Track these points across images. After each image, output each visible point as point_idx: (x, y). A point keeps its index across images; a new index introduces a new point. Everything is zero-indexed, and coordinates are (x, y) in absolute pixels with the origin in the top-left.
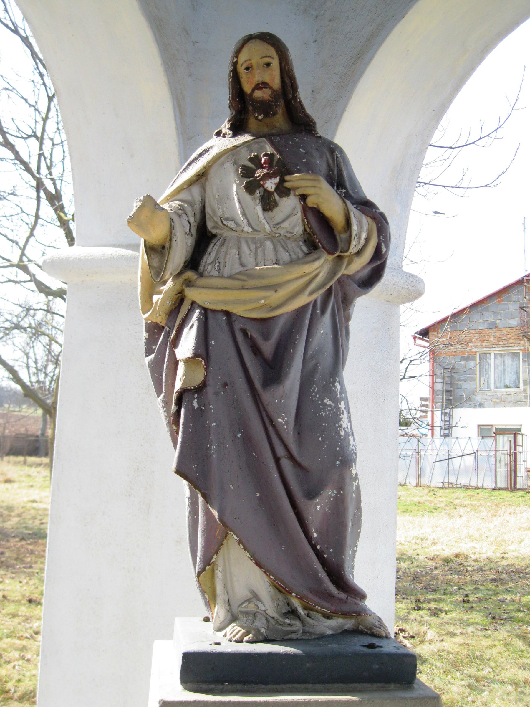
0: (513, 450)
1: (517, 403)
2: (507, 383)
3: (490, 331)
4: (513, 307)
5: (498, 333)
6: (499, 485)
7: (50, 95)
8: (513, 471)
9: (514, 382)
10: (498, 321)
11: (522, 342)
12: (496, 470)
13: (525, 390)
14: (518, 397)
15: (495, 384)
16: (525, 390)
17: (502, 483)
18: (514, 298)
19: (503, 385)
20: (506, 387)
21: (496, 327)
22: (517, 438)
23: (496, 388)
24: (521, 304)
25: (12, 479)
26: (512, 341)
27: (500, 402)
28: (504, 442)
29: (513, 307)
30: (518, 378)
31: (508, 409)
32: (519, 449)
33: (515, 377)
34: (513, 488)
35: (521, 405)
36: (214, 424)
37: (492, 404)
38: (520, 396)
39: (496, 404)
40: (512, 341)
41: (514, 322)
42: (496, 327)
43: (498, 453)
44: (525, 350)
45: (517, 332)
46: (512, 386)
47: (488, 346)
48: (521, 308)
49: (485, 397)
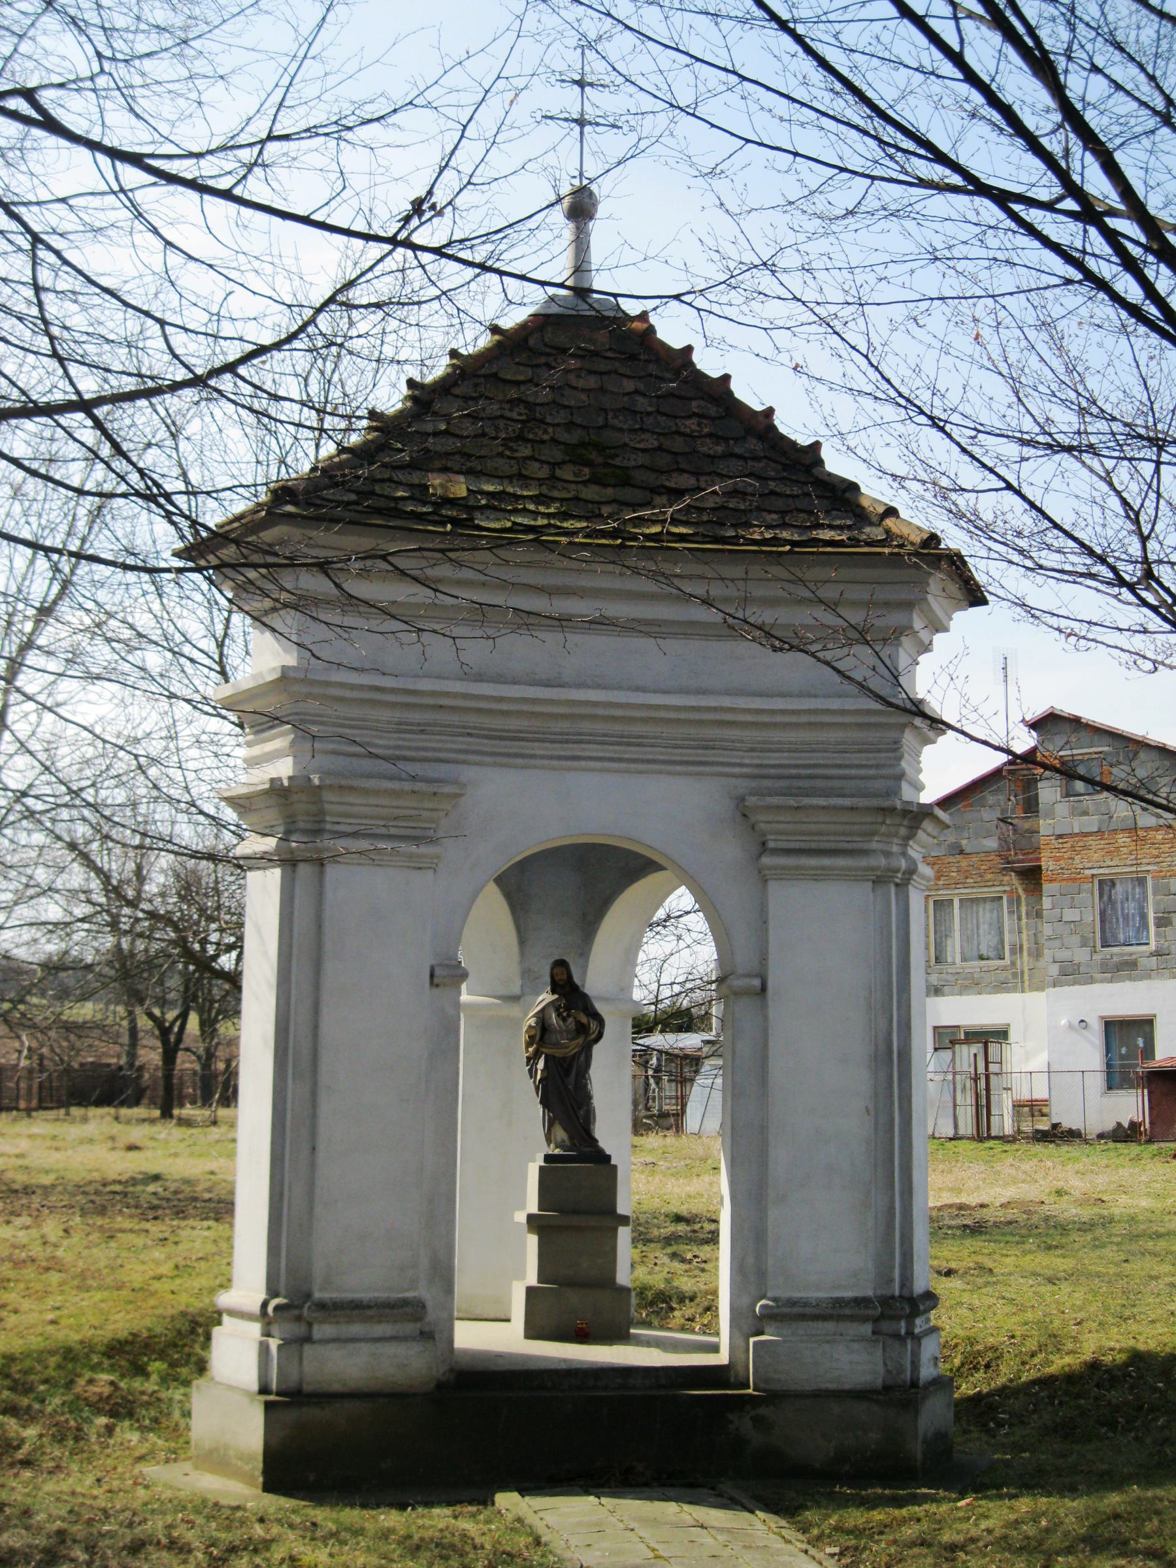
0: (981, 1069)
1: (1001, 987)
2: (984, 952)
3: (951, 859)
4: (990, 815)
5: (964, 864)
6: (962, 1132)
7: (174, 497)
8: (983, 1107)
9: (996, 949)
10: (964, 842)
11: (1006, 878)
12: (955, 1106)
13: (1013, 963)
14: (1003, 976)
15: (962, 953)
16: (1013, 963)
17: (967, 1126)
18: (991, 799)
19: (975, 954)
20: (981, 958)
21: (961, 852)
22: (990, 1050)
23: (964, 959)
24: (1003, 811)
25: (139, 1144)
26: (989, 876)
27: (972, 985)
28: (967, 1054)
29: (990, 815)
30: (1002, 942)
31: (985, 997)
32: (993, 1068)
33: (996, 940)
34: (982, 1134)
35: (1008, 990)
36: (312, 1479)
37: (956, 988)
38: (1005, 974)
39: (963, 990)
40: (989, 876)
41: (992, 844)
42: (961, 852)
43: (958, 1077)
44: (1011, 891)
45: (998, 860)
46: (991, 955)
47: (946, 886)
48: (1002, 820)
49: (944, 976)
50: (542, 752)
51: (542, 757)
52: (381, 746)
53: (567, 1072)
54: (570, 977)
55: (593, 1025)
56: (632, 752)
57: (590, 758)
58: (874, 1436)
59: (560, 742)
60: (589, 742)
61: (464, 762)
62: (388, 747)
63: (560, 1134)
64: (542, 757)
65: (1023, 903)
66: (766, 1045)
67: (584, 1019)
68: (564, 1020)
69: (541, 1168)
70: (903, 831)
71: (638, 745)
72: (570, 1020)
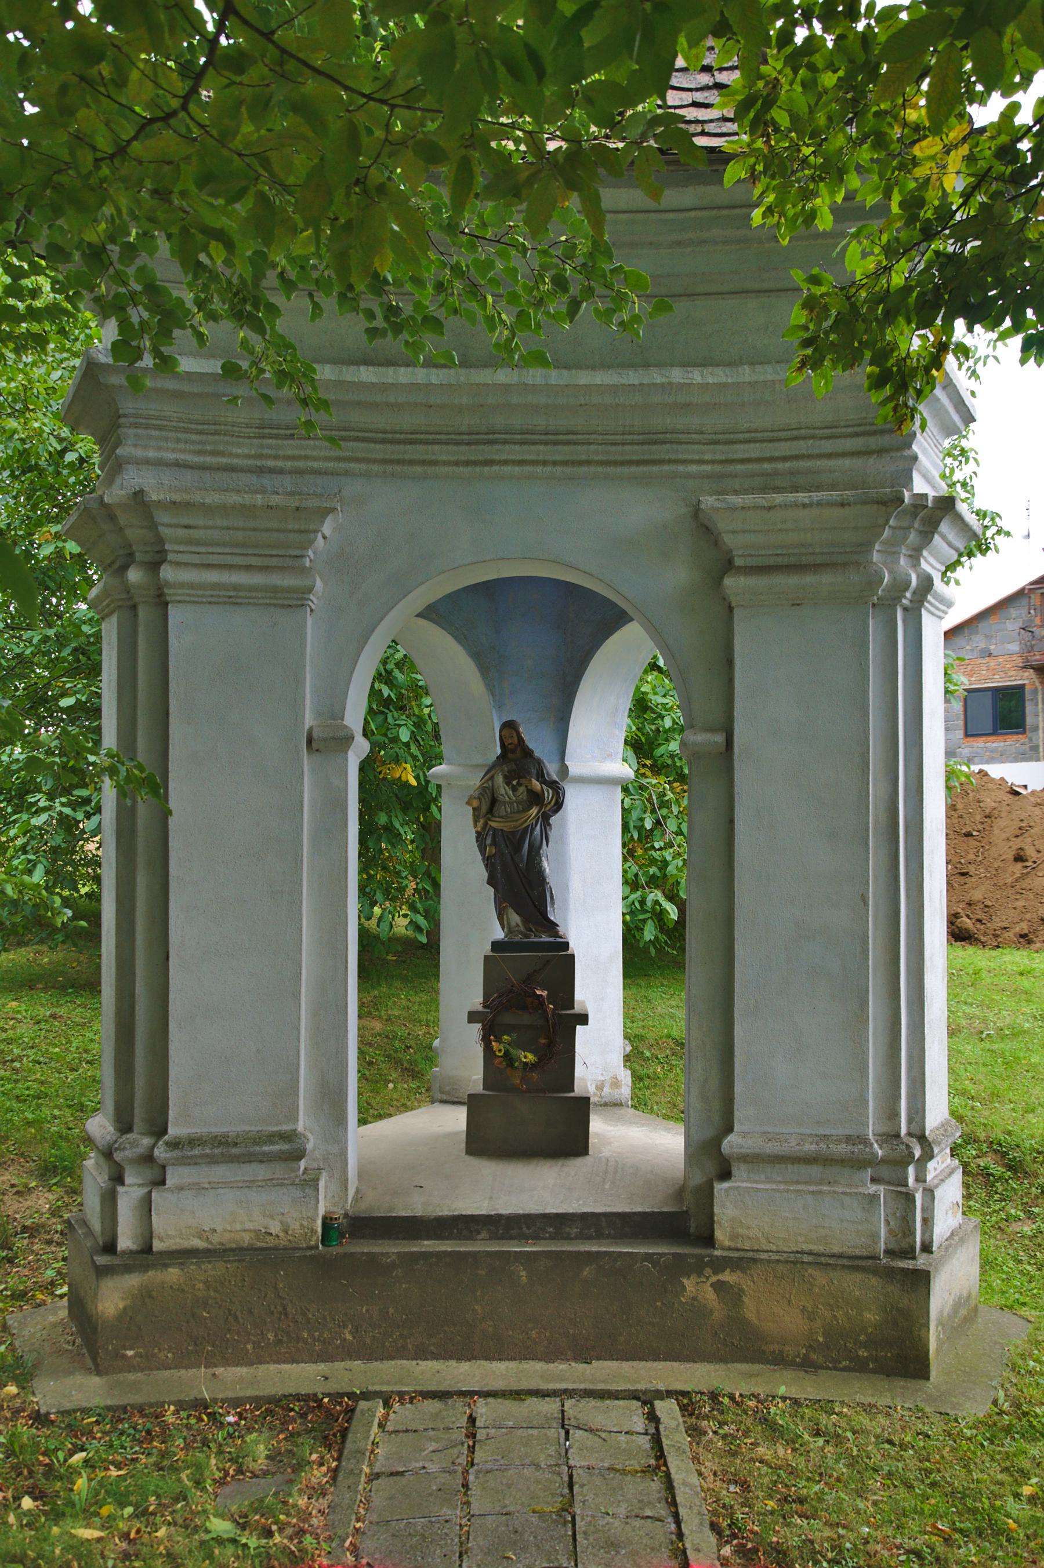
3: (980, 661)
10: (992, 647)
11: (1026, 674)
21: (990, 655)
26: (1013, 673)
40: (1013, 673)
41: (1015, 647)
42: (990, 655)
50: (444, 458)
51: (445, 463)
52: (238, 456)
53: (518, 848)
54: (521, 740)
55: (548, 794)
56: (563, 452)
57: (506, 462)
58: (871, 1316)
59: (469, 444)
60: (505, 442)
61: (347, 473)
62: (247, 456)
63: (515, 918)
64: (445, 463)
65: (740, 1184)
66: (732, 821)
67: (536, 785)
68: (514, 789)
69: (486, 958)
70: (913, 537)
71: (568, 443)
72: (522, 789)
